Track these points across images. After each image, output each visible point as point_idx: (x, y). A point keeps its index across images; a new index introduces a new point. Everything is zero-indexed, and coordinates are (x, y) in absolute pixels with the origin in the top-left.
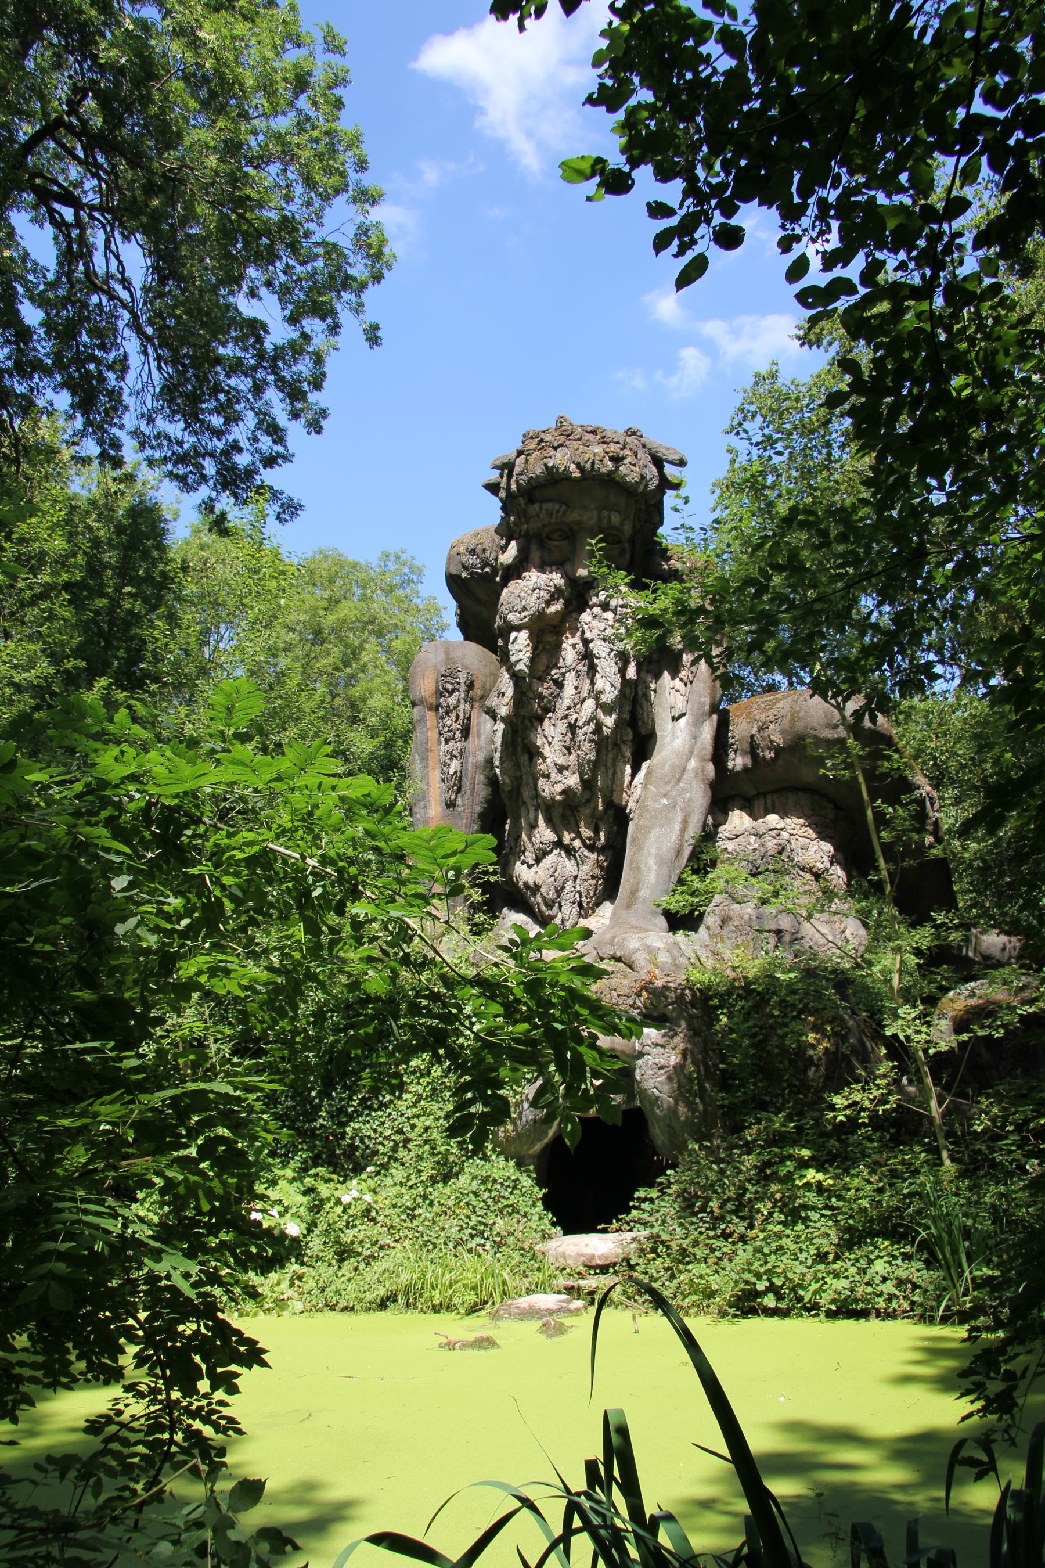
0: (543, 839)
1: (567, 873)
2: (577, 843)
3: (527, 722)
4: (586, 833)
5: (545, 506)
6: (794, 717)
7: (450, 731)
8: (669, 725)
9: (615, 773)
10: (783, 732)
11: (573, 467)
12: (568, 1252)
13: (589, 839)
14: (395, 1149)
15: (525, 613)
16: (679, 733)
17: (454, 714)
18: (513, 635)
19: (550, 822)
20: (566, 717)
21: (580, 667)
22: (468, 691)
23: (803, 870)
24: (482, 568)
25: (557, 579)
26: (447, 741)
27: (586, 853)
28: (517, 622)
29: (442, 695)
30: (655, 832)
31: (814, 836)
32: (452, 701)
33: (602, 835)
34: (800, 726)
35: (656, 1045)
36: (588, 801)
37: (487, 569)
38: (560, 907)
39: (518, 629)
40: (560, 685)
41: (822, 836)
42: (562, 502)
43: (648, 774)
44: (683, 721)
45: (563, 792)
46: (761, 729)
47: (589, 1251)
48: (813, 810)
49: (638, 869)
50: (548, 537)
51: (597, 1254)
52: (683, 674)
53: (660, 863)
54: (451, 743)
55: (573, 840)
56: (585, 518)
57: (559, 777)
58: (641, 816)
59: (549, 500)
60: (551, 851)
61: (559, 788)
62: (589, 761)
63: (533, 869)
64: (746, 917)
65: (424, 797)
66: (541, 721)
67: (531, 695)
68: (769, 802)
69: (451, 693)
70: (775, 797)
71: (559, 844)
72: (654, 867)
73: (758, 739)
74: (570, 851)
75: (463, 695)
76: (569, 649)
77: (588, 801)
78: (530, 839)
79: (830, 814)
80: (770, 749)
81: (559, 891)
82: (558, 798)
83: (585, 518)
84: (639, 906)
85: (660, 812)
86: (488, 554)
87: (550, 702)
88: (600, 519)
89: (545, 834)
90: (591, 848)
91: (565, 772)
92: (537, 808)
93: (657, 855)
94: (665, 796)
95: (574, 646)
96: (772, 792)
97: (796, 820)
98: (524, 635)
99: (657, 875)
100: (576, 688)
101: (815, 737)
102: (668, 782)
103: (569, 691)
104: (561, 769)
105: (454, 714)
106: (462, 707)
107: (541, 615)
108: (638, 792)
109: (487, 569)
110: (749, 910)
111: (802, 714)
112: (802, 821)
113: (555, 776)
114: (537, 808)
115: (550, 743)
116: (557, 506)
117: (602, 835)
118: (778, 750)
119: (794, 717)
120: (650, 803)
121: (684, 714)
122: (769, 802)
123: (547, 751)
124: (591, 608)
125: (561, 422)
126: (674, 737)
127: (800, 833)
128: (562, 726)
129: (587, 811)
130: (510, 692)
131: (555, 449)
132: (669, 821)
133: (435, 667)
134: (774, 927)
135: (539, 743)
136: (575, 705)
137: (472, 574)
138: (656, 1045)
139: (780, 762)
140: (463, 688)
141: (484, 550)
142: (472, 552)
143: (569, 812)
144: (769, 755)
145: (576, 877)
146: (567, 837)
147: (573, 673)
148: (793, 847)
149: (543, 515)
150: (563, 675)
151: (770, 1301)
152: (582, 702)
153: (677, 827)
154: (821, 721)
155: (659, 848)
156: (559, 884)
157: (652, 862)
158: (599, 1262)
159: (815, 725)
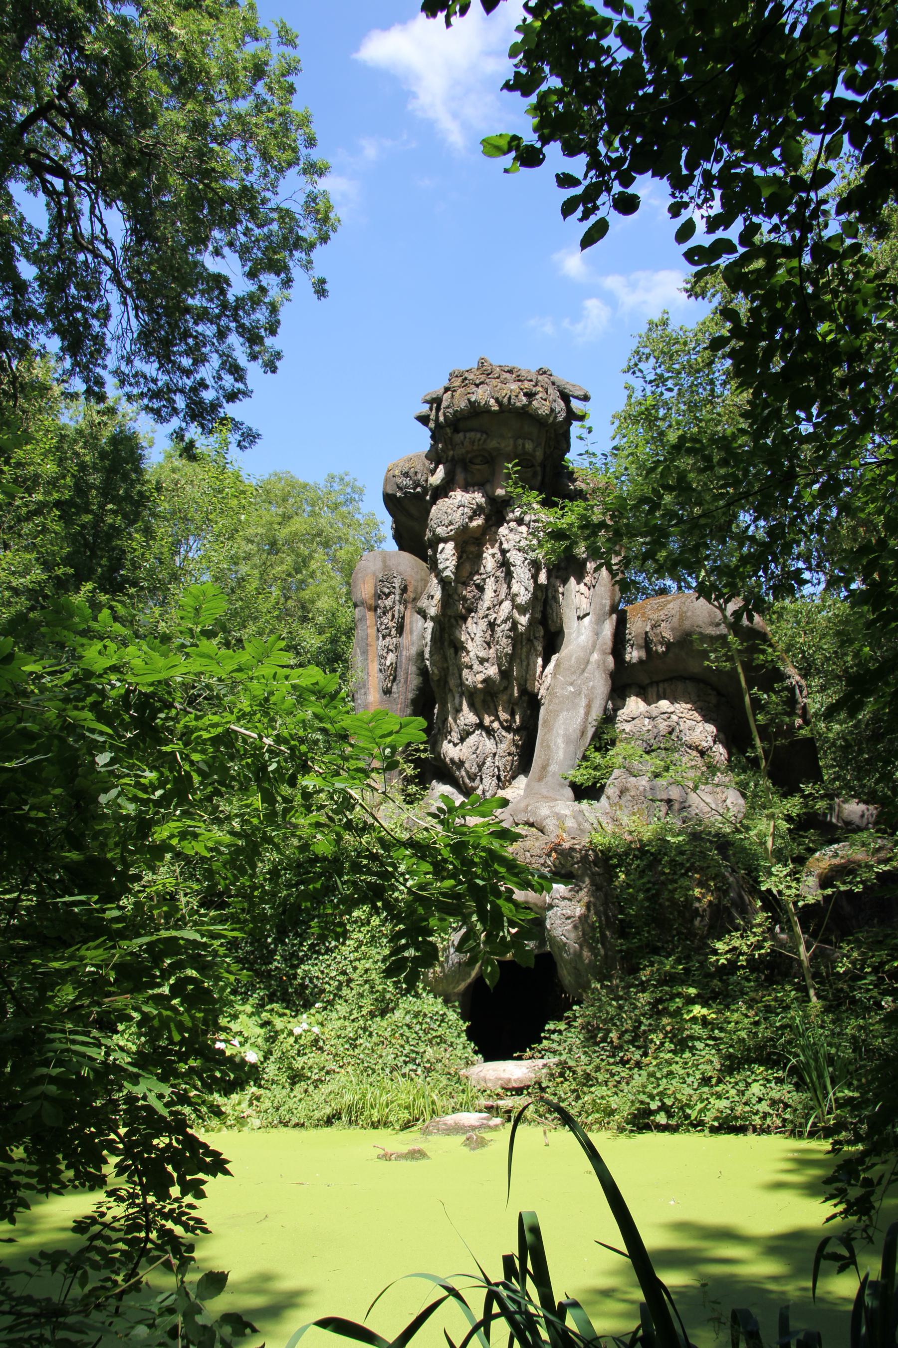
0: (467, 722)
1: (487, 751)
2: (496, 725)
3: (453, 620)
4: (504, 716)
5: (468, 435)
6: (682, 617)
7: (386, 628)
8: (575, 623)
9: (528, 665)
10: (673, 629)
11: (492, 402)
12: (488, 1077)
13: (506, 721)
14: (339, 988)
15: (451, 527)
16: (583, 630)
17: (390, 614)
18: (441, 546)
19: (472, 706)
20: (486, 616)
21: (498, 574)
22: (402, 594)
23: (690, 748)
24: (415, 489)
25: (479, 498)
26: (384, 637)
27: (504, 733)
28: (444, 535)
29: (379, 598)
30: (563, 715)
31: (699, 718)
32: (388, 602)
33: (517, 718)
34: (687, 624)
35: (564, 898)
36: (506, 688)
37: (419, 490)
38: (481, 779)
39: (445, 540)
40: (481, 589)
41: (707, 719)
42: (483, 432)
43: (557, 665)
44: (587, 620)
45: (484, 681)
46: (654, 627)
47: (506, 1076)
48: (699, 696)
49: (549, 747)
50: (471, 462)
51: (513, 1078)
52: (587, 580)
53: (568, 742)
54: (388, 639)
55: (492, 722)
56: (503, 445)
57: (481, 668)
58: (551, 701)
59: (471, 430)
60: (474, 732)
61: (480, 677)
62: (507, 654)
63: (458, 747)
64: (641, 788)
65: (364, 685)
66: (465, 620)
67: (456, 598)
68: (661, 690)
69: (388, 595)
70: (666, 685)
71: (480, 726)
72: (562, 746)
73: (651, 635)
74: (490, 732)
75: (397, 598)
76: (489, 558)
77: (506, 688)
78: (455, 721)
79: (713, 699)
80: (662, 644)
81: (480, 766)
82: (480, 686)
83: (503, 445)
84: (549, 779)
85: (568, 698)
86: (419, 476)
87: (472, 603)
88: (515, 446)
89: (468, 717)
90: (508, 729)
91: (486, 664)
92: (462, 695)
93: (565, 735)
94: (572, 684)
95: (493, 555)
96: (664, 681)
97: (684, 705)
98: (450, 546)
99: (565, 752)
100: (495, 591)
101: (701, 633)
102: (574, 673)
103: (489, 594)
104: (482, 661)
105: (390, 614)
106: (397, 608)
107: (465, 528)
108: (548, 681)
109: (419, 490)
110: (644, 783)
111: (689, 614)
112: (689, 706)
113: (477, 667)
114: (462, 695)
115: (472, 639)
116: (478, 435)
117: (517, 718)
118: (669, 645)
119: (682, 617)
120: (558, 690)
121: (588, 614)
122: (661, 690)
123: (470, 646)
124: (508, 523)
125: (482, 363)
126: (579, 634)
127: (688, 716)
128: (483, 624)
129: (505, 698)
130: (438, 595)
131: (477, 386)
132: (575, 706)
133: (374, 574)
134: (665, 797)
135: (463, 638)
136: (494, 606)
137: (405, 493)
138: (564, 898)
139: (670, 655)
140: (398, 591)
141: (416, 473)
142: (406, 475)
143: (489, 698)
144: (661, 649)
145: (495, 754)
146: (487, 720)
147: (493, 579)
148: (682, 728)
149: (466, 443)
150: (484, 580)
151: (661, 1118)
152: (500, 603)
153: (582, 711)
154: (706, 620)
155: (566, 729)
156: (480, 760)
157: (560, 741)
158: (515, 1085)
159: (700, 623)
